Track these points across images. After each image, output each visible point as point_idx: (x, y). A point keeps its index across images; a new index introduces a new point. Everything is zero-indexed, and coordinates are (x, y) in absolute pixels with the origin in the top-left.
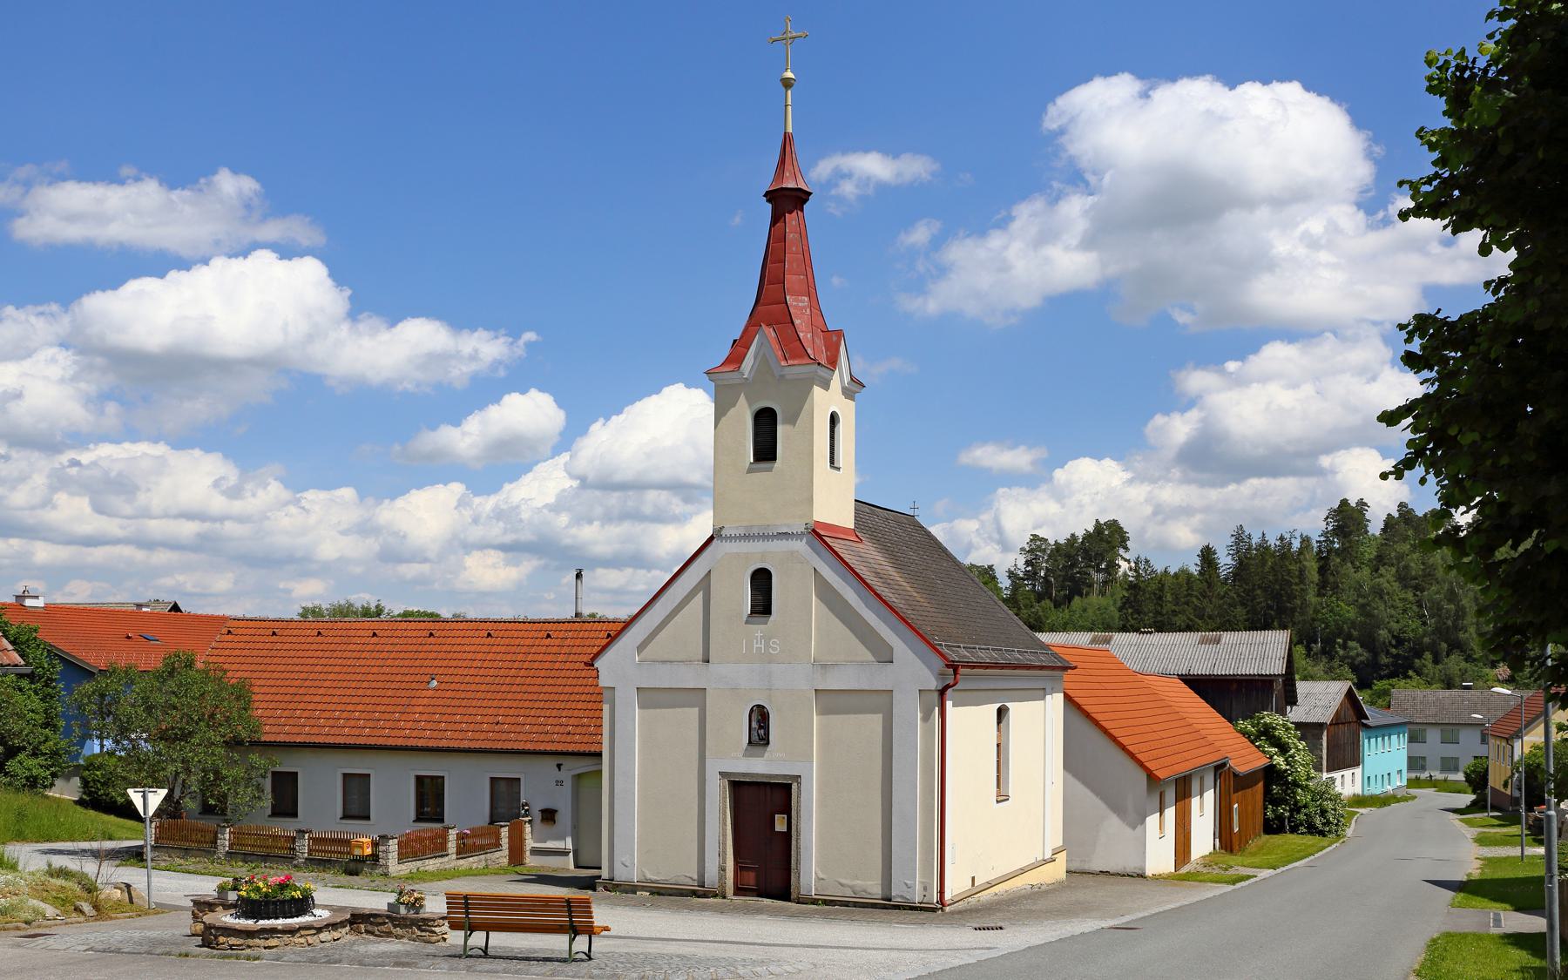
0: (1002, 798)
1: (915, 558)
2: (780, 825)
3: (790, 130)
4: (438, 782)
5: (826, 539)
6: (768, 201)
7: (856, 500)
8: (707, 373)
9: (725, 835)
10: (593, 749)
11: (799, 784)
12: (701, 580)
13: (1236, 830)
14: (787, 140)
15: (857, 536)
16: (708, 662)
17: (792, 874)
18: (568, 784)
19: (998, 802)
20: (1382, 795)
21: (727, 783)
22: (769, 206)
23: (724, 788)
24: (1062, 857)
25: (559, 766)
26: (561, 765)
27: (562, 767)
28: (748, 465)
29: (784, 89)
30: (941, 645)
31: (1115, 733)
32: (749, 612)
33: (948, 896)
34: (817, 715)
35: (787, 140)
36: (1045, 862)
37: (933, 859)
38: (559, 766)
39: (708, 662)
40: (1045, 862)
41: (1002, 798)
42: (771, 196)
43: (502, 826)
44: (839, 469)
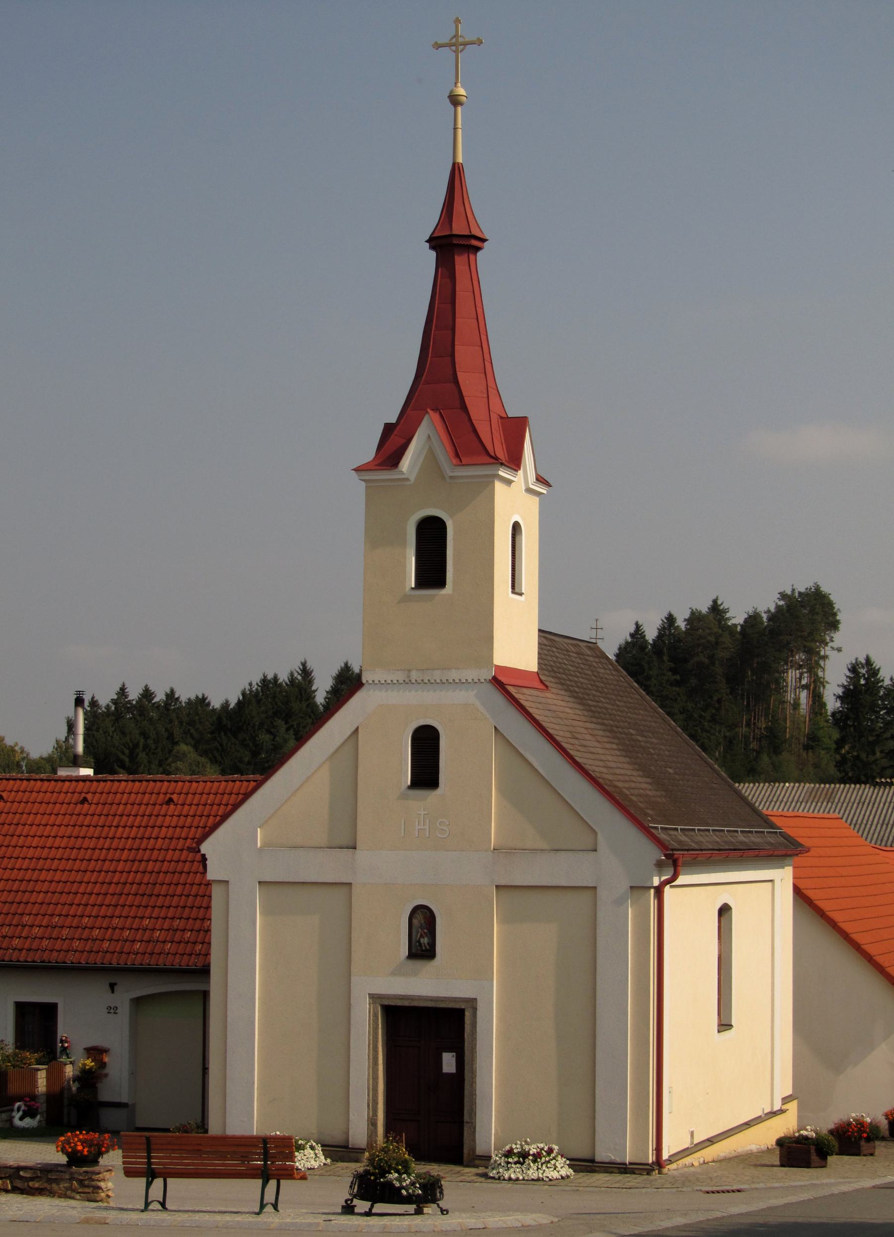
0: (724, 1025)
1: (594, 692)
2: (449, 1062)
3: (460, 160)
4: (49, 1012)
5: (511, 689)
6: (432, 248)
7: (540, 631)
8: (357, 470)
9: (375, 1079)
10: (194, 962)
11: (475, 1009)
12: (346, 740)
13: (287, 1163)
14: (456, 172)
15: (541, 681)
16: (355, 848)
17: (465, 1129)
18: (125, 1009)
19: (719, 1032)
20: (519, 1213)
21: (379, 1008)
22: (433, 254)
23: (376, 1015)
24: (793, 1106)
25: (112, 986)
26: (115, 984)
27: (116, 987)
28: (408, 588)
29: (452, 107)
30: (656, 828)
31: (836, 916)
32: (409, 783)
33: (665, 1156)
34: (501, 921)
35: (456, 172)
36: (773, 1114)
37: (648, 1106)
38: (112, 986)
39: (355, 848)
40: (773, 1114)
41: (724, 1025)
42: (434, 242)
43: (39, 1070)
44: (521, 594)
